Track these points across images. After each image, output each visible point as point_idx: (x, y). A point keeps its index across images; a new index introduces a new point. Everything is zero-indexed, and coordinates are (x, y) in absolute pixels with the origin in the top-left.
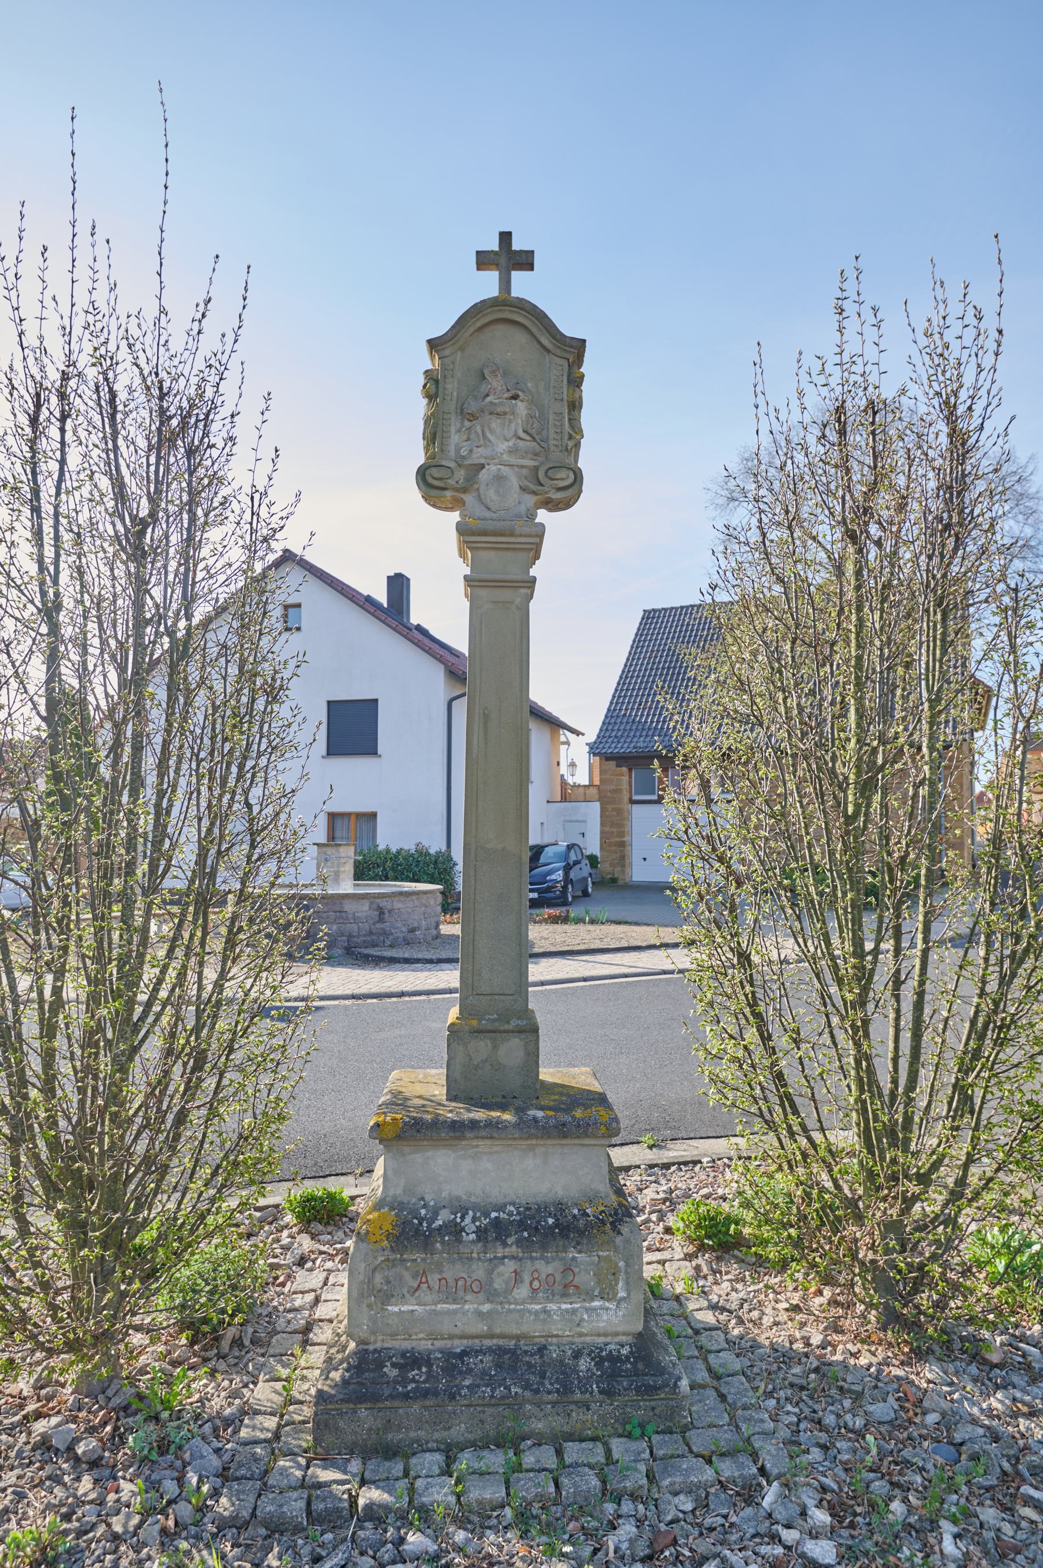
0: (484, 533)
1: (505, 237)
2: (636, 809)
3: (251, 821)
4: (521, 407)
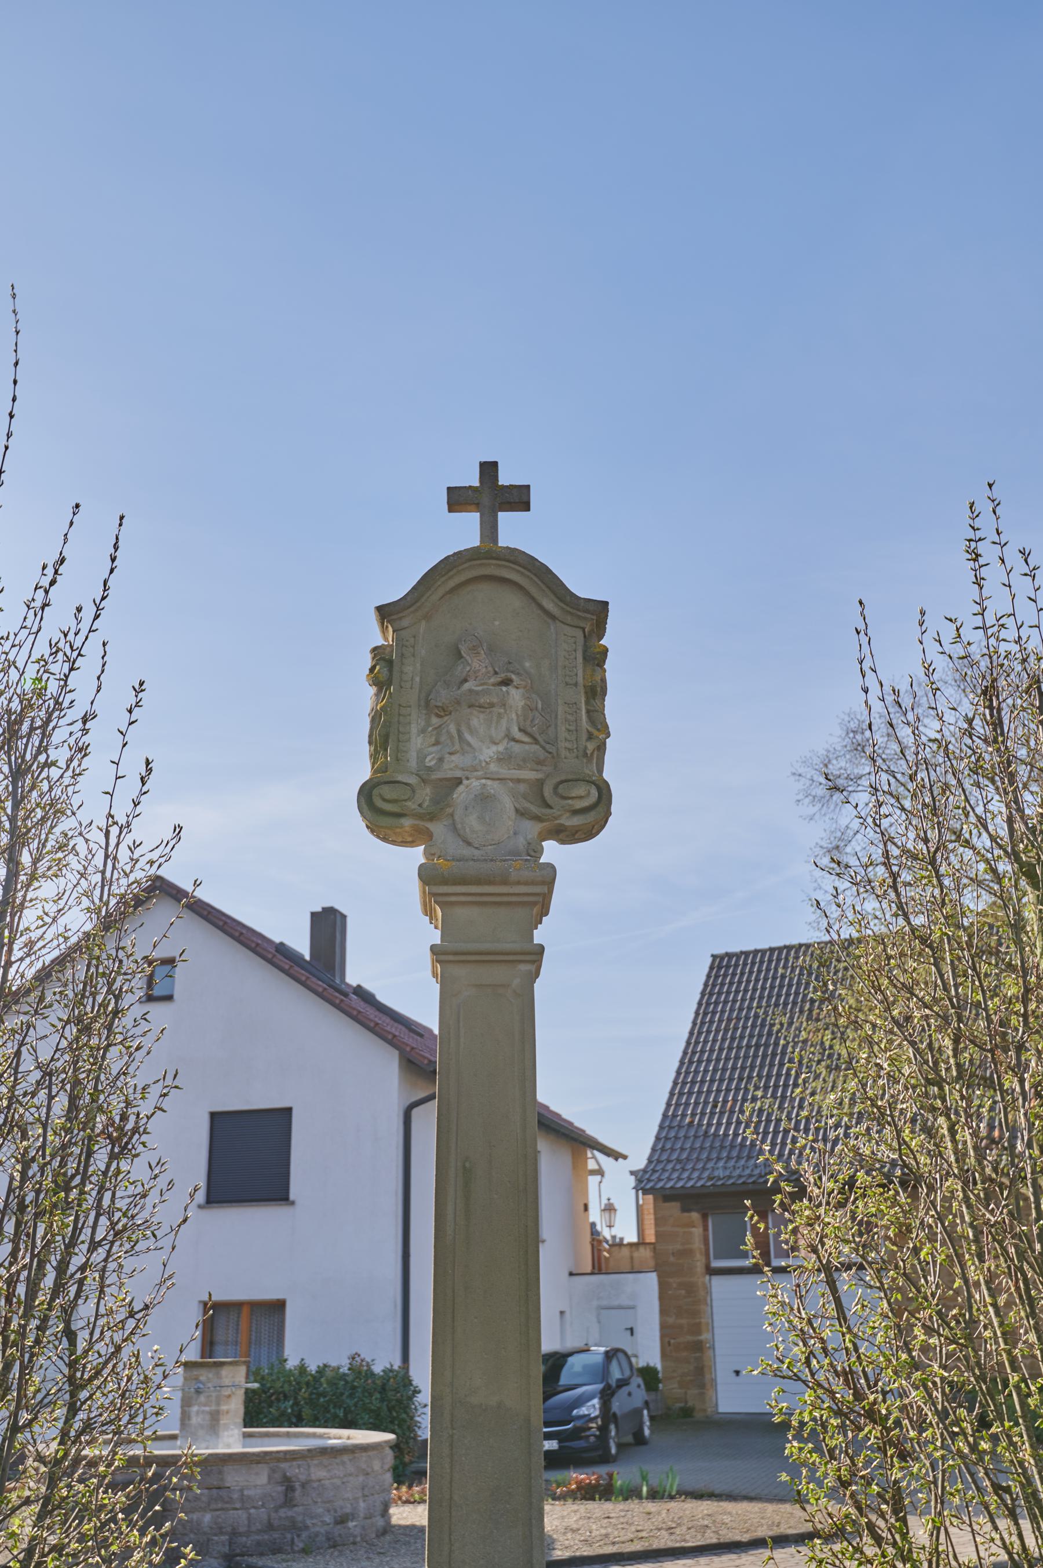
0: (464, 881)
1: (489, 469)
2: (719, 1286)
3: (72, 1365)
4: (516, 697)
